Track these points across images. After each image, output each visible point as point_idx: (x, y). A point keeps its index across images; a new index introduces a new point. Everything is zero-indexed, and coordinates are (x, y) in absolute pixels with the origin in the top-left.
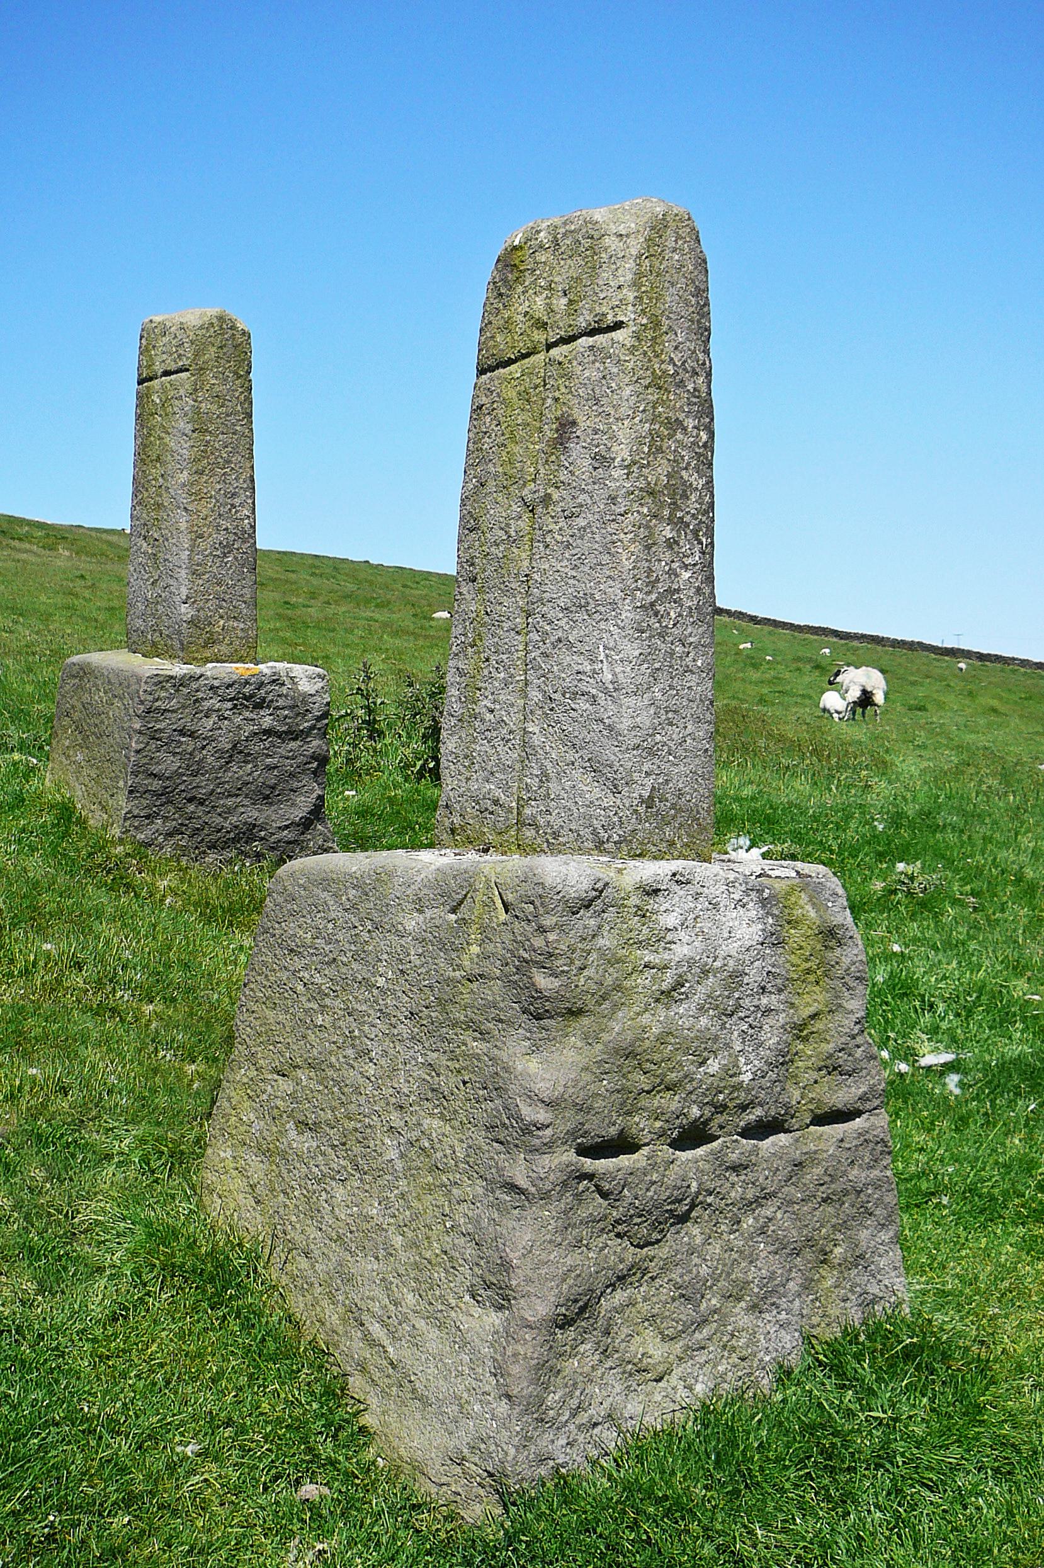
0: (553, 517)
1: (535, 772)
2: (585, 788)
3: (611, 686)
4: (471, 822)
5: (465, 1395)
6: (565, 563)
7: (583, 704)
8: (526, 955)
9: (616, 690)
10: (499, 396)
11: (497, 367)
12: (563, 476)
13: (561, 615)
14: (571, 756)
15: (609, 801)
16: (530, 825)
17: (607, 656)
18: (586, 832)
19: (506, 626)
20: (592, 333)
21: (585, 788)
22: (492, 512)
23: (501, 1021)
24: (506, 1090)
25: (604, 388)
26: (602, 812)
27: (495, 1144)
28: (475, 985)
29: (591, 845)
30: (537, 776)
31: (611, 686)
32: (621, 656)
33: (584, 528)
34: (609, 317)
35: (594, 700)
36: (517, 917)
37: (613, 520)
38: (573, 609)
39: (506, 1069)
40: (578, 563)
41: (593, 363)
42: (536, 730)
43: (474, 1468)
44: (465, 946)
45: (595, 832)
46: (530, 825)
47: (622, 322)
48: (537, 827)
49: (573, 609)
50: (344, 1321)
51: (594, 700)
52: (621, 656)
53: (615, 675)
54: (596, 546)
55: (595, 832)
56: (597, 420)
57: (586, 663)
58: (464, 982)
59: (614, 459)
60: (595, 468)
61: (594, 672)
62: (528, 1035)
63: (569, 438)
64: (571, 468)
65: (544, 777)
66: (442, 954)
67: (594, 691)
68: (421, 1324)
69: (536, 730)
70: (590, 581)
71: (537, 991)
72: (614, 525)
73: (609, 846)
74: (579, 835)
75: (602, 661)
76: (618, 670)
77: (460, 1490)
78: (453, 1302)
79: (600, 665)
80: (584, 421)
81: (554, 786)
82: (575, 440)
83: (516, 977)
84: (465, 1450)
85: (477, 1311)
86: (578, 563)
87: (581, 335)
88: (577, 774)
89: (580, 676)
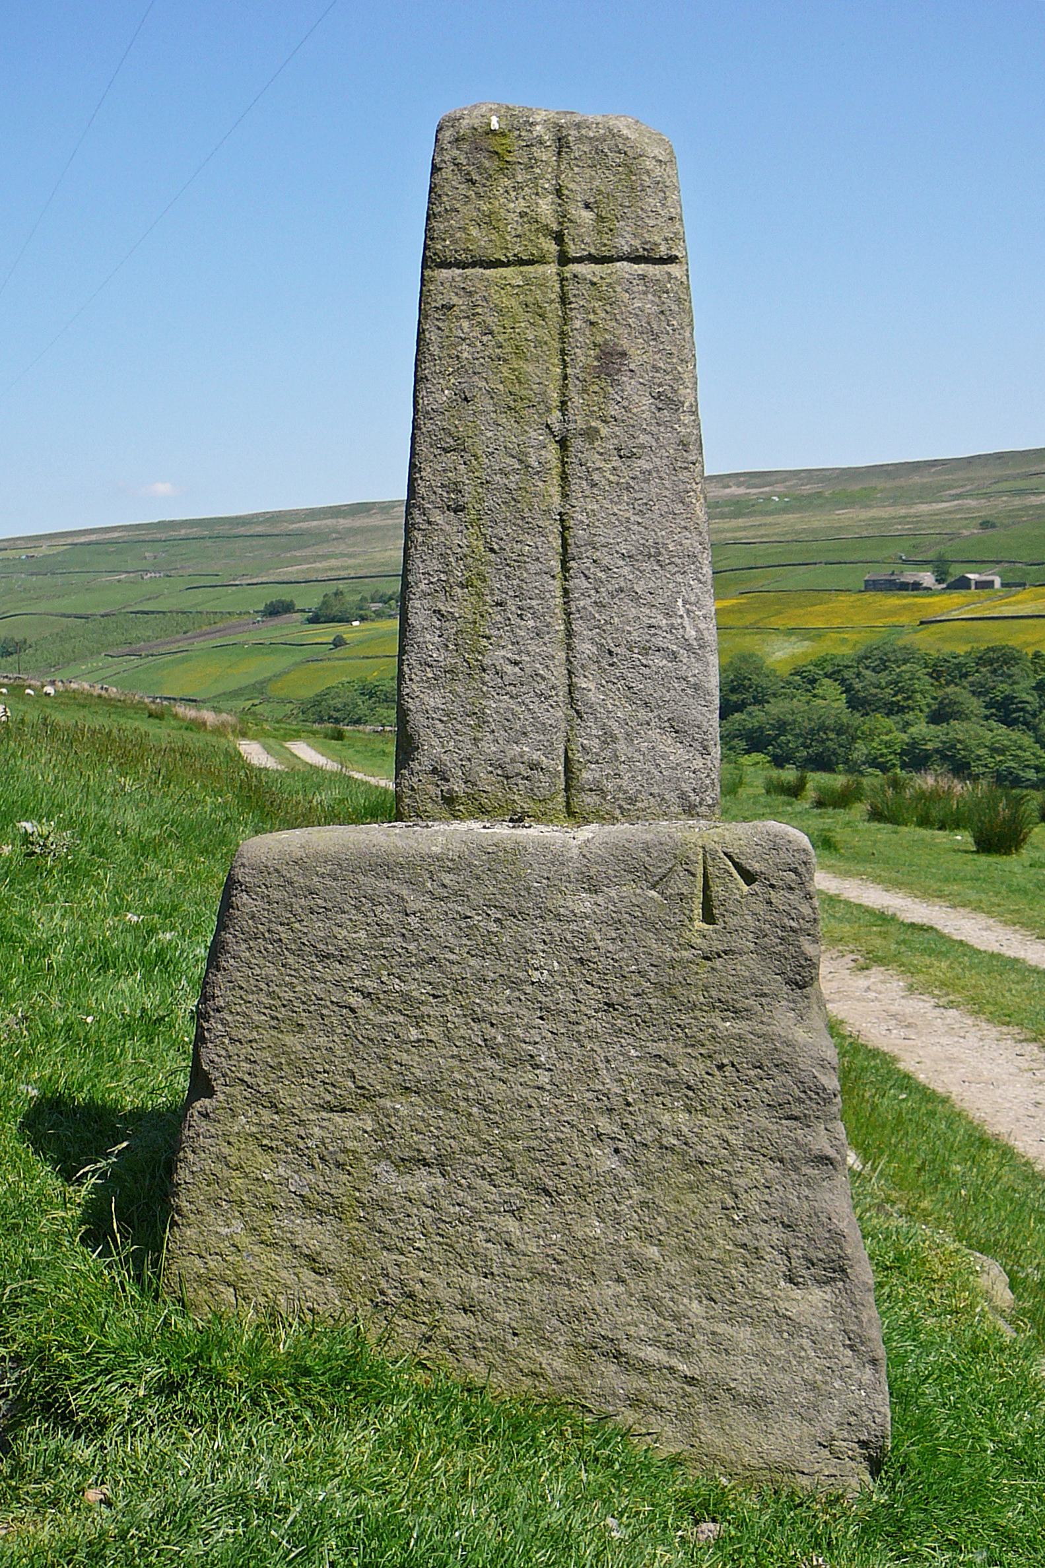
0: (601, 454)
1: (594, 732)
2: (667, 750)
3: (695, 643)
4: (488, 788)
5: (819, 1377)
6: (624, 507)
7: (658, 661)
8: (794, 924)
9: (701, 647)
10: (485, 299)
11: (474, 265)
12: (613, 410)
13: (621, 563)
14: (643, 715)
15: (698, 763)
16: (591, 790)
17: (688, 611)
18: (671, 797)
19: (533, 568)
20: (637, 260)
21: (667, 750)
22: (489, 434)
23: (764, 995)
24: (793, 1066)
25: (664, 324)
26: (692, 775)
27: (783, 1121)
28: (718, 963)
29: (680, 810)
30: (598, 737)
31: (695, 643)
32: (704, 612)
33: (650, 473)
34: (663, 248)
35: (674, 657)
36: (772, 886)
37: (686, 468)
38: (640, 557)
39: (787, 1043)
40: (644, 508)
41: (645, 293)
42: (592, 686)
43: (845, 1444)
44: (687, 922)
45: (683, 796)
46: (591, 790)
47: (676, 257)
48: (602, 792)
49: (640, 557)
50: (578, 1361)
51: (674, 657)
52: (704, 612)
53: (698, 630)
54: (667, 493)
55: (683, 796)
56: (657, 357)
57: (660, 617)
58: (699, 960)
59: (683, 403)
60: (660, 409)
61: (672, 626)
62: (792, 1005)
63: (619, 370)
64: (626, 404)
65: (608, 738)
66: (651, 935)
67: (675, 648)
68: (721, 1328)
69: (592, 686)
70: (661, 530)
71: (806, 959)
72: (686, 473)
73: (702, 810)
74: (663, 799)
75: (681, 617)
76: (702, 626)
77: (834, 1472)
78: (768, 1293)
79: (679, 621)
80: (639, 354)
81: (622, 746)
82: (629, 373)
83: (780, 948)
84: (835, 1430)
85: (797, 1294)
86: (644, 508)
87: (620, 259)
88: (654, 734)
89: (653, 631)
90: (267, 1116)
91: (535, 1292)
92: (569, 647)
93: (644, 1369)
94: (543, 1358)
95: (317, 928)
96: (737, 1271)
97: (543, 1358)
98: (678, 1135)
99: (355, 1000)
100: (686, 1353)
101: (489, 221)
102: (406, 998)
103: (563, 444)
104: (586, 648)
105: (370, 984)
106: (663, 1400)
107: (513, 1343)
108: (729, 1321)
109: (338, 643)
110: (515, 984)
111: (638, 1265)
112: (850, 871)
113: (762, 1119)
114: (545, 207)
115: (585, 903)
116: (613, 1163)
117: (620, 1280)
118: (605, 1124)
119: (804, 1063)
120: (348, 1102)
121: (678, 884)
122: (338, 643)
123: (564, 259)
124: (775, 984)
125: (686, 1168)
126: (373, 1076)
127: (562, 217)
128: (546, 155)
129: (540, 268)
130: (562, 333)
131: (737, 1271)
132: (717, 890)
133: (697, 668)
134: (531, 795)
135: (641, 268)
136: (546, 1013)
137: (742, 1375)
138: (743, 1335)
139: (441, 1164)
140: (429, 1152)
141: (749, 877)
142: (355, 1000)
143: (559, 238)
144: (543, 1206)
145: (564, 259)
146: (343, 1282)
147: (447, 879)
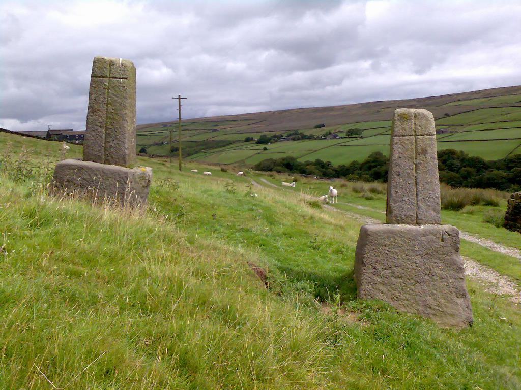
90: (374, 270)
91: (417, 298)
92: (417, 198)
93: (434, 310)
94: (419, 307)
95: (382, 241)
96: (449, 295)
97: (419, 307)
98: (439, 274)
99: (388, 253)
100: (441, 307)
101: (403, 129)
102: (396, 252)
103: (416, 165)
104: (420, 198)
105: (390, 250)
106: (437, 315)
107: (413, 305)
108: (448, 303)
109: (265, 149)
110: (413, 251)
111: (433, 294)
112: (362, 190)
113: (452, 272)
114: (413, 126)
115: (424, 238)
116: (429, 278)
117: (430, 296)
118: (427, 272)
119: (458, 264)
120: (387, 268)
121: (438, 236)
122: (265, 149)
123: (416, 135)
124: (453, 251)
125: (440, 279)
126: (391, 264)
127: (416, 128)
128: (413, 118)
129: (412, 137)
130: (259, 142)
131: (449, 295)
132: (444, 237)
133: (437, 200)
134: (411, 220)
135: (429, 136)
136: (418, 255)
137: (449, 311)
138: (450, 305)
139: (402, 278)
140: (400, 276)
141: (449, 235)
142: (388, 253)
143: (415, 131)
144: (418, 285)
145: (416, 135)
146: (387, 295)
147: (402, 234)
